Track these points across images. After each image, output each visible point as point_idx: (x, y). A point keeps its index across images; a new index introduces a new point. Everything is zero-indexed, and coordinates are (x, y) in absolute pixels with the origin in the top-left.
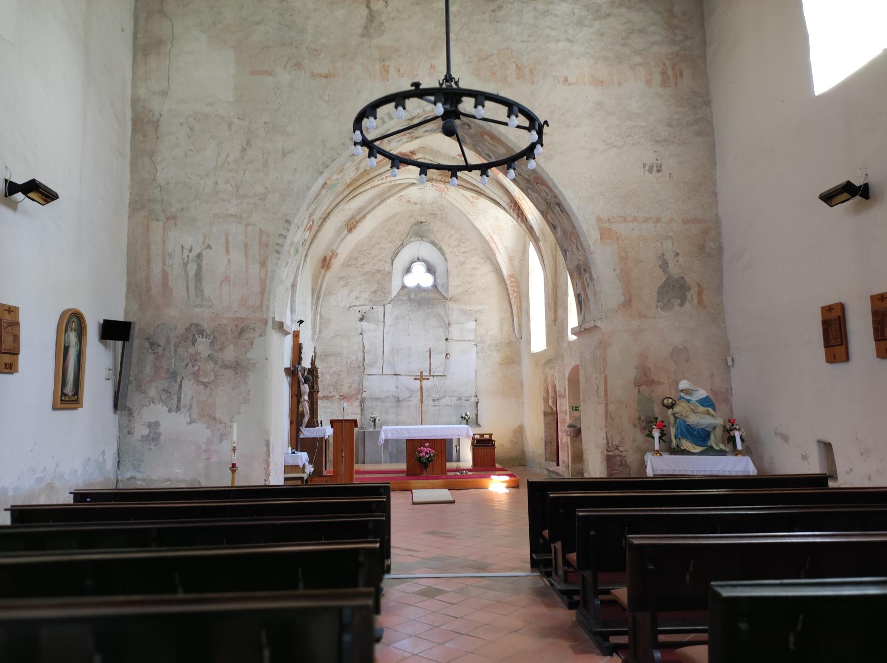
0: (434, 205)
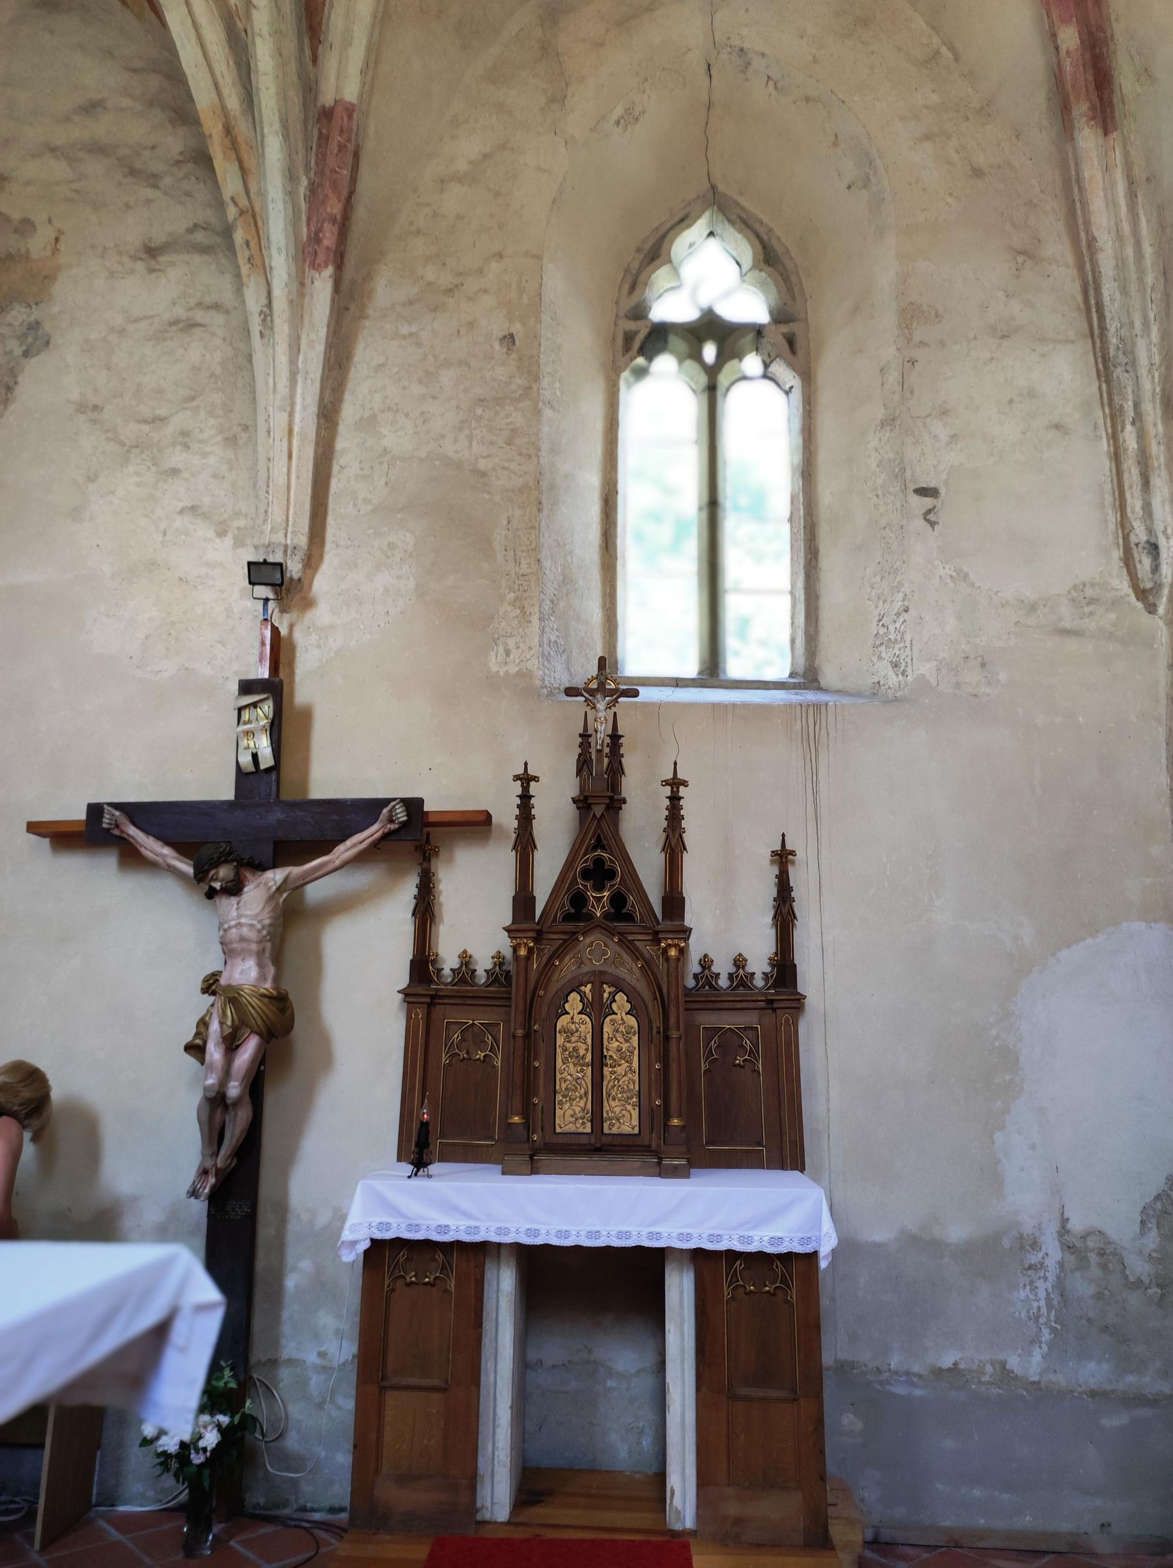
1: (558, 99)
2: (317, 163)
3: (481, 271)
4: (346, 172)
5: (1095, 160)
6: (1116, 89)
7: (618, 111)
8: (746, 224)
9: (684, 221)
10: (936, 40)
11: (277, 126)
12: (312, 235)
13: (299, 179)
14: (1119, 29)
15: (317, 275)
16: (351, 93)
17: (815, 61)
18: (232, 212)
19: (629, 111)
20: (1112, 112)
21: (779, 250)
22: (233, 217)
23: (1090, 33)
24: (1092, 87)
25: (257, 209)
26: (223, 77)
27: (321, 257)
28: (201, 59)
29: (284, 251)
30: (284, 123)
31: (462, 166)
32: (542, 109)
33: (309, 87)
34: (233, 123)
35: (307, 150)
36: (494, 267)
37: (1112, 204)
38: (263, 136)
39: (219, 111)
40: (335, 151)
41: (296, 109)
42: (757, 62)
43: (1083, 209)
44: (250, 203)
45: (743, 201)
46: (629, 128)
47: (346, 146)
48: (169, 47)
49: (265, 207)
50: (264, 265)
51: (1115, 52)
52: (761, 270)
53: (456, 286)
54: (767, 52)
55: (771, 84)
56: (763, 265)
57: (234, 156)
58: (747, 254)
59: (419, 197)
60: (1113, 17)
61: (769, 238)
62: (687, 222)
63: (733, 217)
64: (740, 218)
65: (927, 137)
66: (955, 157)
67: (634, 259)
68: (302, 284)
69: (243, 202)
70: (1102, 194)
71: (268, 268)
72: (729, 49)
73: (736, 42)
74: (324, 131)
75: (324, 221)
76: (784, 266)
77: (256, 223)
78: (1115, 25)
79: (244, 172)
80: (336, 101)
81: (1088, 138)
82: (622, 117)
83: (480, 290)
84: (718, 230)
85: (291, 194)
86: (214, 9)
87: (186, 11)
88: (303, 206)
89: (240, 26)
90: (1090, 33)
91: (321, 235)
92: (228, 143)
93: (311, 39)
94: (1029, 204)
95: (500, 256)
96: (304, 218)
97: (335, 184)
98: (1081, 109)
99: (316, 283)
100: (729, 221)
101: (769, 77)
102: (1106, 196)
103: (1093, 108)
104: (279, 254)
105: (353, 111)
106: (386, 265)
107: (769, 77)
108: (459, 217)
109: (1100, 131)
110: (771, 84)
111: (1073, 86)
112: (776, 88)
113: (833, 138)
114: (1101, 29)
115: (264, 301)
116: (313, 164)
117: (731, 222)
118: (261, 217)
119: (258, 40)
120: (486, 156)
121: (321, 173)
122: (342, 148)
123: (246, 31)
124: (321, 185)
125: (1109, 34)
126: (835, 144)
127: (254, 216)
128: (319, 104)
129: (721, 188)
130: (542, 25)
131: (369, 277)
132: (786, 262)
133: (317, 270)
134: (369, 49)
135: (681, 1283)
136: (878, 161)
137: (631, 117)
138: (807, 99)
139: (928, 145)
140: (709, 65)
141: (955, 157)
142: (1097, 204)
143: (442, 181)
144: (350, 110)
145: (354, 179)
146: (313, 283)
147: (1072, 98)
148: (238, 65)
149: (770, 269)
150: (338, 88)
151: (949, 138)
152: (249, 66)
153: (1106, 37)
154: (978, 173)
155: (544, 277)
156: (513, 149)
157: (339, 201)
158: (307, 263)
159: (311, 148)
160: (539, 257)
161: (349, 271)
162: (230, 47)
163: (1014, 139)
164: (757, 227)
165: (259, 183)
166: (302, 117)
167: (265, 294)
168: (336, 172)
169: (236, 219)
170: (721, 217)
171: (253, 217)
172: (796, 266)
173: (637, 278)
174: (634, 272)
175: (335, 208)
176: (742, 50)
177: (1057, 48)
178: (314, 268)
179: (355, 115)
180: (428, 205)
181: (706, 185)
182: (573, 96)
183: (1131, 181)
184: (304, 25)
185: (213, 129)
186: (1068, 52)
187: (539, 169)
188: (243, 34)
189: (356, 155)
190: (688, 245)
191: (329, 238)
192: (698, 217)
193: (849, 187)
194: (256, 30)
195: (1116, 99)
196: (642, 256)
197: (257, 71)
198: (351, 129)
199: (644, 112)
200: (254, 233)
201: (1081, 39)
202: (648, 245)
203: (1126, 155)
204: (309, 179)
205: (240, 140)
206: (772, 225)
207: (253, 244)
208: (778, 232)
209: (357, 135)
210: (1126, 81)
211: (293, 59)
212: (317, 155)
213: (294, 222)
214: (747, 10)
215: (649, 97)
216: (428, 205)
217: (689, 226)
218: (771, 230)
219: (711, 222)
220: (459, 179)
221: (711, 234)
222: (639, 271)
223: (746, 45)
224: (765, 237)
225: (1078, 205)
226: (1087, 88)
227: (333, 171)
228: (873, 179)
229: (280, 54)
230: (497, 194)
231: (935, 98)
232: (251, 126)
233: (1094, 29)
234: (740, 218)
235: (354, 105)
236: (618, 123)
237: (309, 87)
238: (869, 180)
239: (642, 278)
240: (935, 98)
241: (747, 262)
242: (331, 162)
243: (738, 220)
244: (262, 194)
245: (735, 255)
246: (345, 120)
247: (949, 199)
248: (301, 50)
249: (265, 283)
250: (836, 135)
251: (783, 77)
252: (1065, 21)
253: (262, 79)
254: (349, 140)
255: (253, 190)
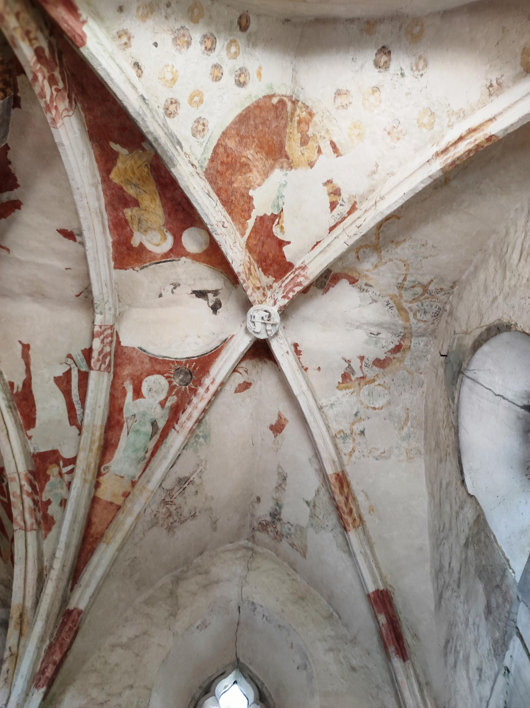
0: (406, 306)
1: (173, 615)
2: (57, 634)
3: (120, 694)
4: (68, 640)
5: (402, 673)
6: (405, 641)
7: (199, 622)
8: (252, 679)
9: (223, 675)
10: (331, 609)
11: (44, 617)
12: (42, 669)
13: (45, 641)
14: (402, 616)
15: (36, 691)
16: (82, 606)
17: (283, 611)
18: (7, 654)
19: (203, 623)
20: (405, 651)
21: (267, 694)
22: (6, 657)
23: (390, 618)
24: (395, 640)
25: (20, 653)
26: (29, 593)
27: (42, 681)
28: (22, 585)
29: (24, 677)
30: (48, 616)
31: (124, 640)
32: (166, 618)
33: (65, 600)
34: (25, 612)
35: (54, 627)
36: (128, 692)
37: (413, 694)
38: (36, 621)
39: (21, 607)
40: (67, 630)
41: (56, 610)
42: (259, 609)
43: (401, 695)
44: (18, 650)
45: (251, 668)
46: (202, 630)
47: (73, 628)
48: (11, 574)
49: (24, 653)
50: (12, 683)
51: (402, 626)
52: (258, 704)
53: (106, 702)
54: (263, 605)
55: (265, 618)
56: (259, 702)
57: (19, 627)
58: (252, 695)
59: (100, 653)
60: (398, 612)
61: (262, 688)
62: (225, 675)
63: (246, 675)
64: (249, 676)
65: (331, 650)
66: (343, 660)
67: (197, 692)
68: (27, 695)
69: (14, 650)
70: (408, 689)
71: (13, 684)
72: (247, 602)
73: (251, 599)
74: (65, 620)
75: (50, 663)
76: (269, 704)
77: (16, 660)
78: (400, 615)
79: (21, 634)
80: (75, 608)
81: (397, 662)
82: (200, 625)
83: (118, 705)
84: (239, 680)
85: (39, 648)
86: (36, 566)
87: (24, 566)
88: (43, 654)
89: (45, 573)
90: (390, 618)
91: (46, 670)
92: (19, 621)
93: (73, 581)
94: (378, 687)
95: (131, 687)
96: (41, 660)
97: (61, 646)
98: (392, 649)
99: (35, 695)
100: (244, 676)
101: (264, 615)
102: (410, 690)
103: (396, 649)
104: (22, 678)
105: (81, 613)
106: (74, 686)
107: (264, 615)
108: (117, 665)
109: (401, 660)
110: (265, 618)
111: (387, 639)
112: (267, 620)
113: (290, 645)
114: (394, 616)
115: (5, 702)
116: (55, 635)
117: (245, 678)
118: (20, 657)
119: (50, 581)
120: (136, 636)
121: (57, 639)
122: (70, 629)
123: (46, 575)
124: (55, 645)
125: (398, 618)
126: (292, 647)
127: (17, 658)
128: (67, 608)
129: (241, 660)
130: (172, 584)
131: (63, 692)
132: (269, 700)
133: (131, 374)
134: (96, 589)
135: (375, 582)
136: (310, 659)
137: (204, 625)
138: (280, 626)
139: (331, 654)
140: (239, 607)
141: (343, 660)
142: (407, 694)
143: (113, 646)
144: (80, 613)
145: (72, 643)
146: (33, 695)
147: (387, 644)
148: (38, 588)
149: (262, 704)
150: (77, 603)
151: (340, 651)
152: (42, 589)
153: (397, 620)
154: (353, 669)
155: (151, 700)
156: (149, 635)
157: (61, 654)
158: (34, 684)
159: (57, 627)
160: (150, 689)
161: (54, 688)
162: (37, 581)
163: (367, 655)
164: (257, 681)
165: (26, 641)
166: (57, 613)
167: (6, 697)
168: (64, 640)
169: (7, 658)
170: (241, 674)
171: (16, 657)
172: (274, 704)
173: (197, 702)
174: (197, 699)
175: (57, 657)
176: (253, 603)
177: (378, 622)
178: (36, 687)
179: (81, 615)
180: (104, 657)
181: (234, 658)
182: (180, 614)
183: (419, 684)
184: (72, 576)
185: (15, 614)
186: (383, 625)
187: (160, 645)
188: (45, 576)
189: (76, 632)
190: (224, 687)
191: (49, 673)
192: (230, 673)
193: (298, 668)
194: (51, 577)
195: (406, 646)
196: (201, 691)
197: (44, 593)
198: (77, 621)
199: (210, 624)
200: (13, 666)
201: (387, 620)
202: (205, 685)
203: (415, 671)
204: (50, 641)
205: (25, 620)
206: (264, 682)
207: (11, 672)
208: (266, 685)
209: (80, 623)
210: (408, 638)
211: (62, 589)
212: (58, 630)
213: (35, 664)
214: (256, 587)
215: (213, 618)
216: (104, 657)
217: (226, 677)
218: (263, 684)
219: (236, 677)
220: (123, 646)
221: (235, 682)
222: (199, 699)
223: (255, 601)
224: (260, 687)
225: (399, 692)
226: (393, 641)
227: (63, 639)
228: (308, 666)
229: (57, 587)
230: (137, 655)
231: (333, 633)
232: (33, 614)
233: (392, 617)
234: (249, 676)
235: (82, 611)
236: (198, 627)
237: (65, 600)
238: (306, 666)
239: (200, 703)
240: (333, 633)
241: (252, 700)
242: (63, 635)
243: (248, 677)
244: (25, 646)
245: (246, 694)
246: (76, 617)
247: (342, 680)
248: (67, 585)
249: (8, 693)
250: (292, 644)
251: (270, 616)
252: (380, 612)
253: (45, 596)
254: (75, 626)
255: (22, 643)
